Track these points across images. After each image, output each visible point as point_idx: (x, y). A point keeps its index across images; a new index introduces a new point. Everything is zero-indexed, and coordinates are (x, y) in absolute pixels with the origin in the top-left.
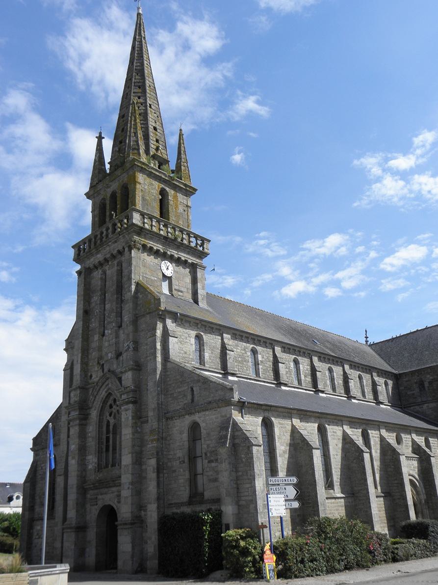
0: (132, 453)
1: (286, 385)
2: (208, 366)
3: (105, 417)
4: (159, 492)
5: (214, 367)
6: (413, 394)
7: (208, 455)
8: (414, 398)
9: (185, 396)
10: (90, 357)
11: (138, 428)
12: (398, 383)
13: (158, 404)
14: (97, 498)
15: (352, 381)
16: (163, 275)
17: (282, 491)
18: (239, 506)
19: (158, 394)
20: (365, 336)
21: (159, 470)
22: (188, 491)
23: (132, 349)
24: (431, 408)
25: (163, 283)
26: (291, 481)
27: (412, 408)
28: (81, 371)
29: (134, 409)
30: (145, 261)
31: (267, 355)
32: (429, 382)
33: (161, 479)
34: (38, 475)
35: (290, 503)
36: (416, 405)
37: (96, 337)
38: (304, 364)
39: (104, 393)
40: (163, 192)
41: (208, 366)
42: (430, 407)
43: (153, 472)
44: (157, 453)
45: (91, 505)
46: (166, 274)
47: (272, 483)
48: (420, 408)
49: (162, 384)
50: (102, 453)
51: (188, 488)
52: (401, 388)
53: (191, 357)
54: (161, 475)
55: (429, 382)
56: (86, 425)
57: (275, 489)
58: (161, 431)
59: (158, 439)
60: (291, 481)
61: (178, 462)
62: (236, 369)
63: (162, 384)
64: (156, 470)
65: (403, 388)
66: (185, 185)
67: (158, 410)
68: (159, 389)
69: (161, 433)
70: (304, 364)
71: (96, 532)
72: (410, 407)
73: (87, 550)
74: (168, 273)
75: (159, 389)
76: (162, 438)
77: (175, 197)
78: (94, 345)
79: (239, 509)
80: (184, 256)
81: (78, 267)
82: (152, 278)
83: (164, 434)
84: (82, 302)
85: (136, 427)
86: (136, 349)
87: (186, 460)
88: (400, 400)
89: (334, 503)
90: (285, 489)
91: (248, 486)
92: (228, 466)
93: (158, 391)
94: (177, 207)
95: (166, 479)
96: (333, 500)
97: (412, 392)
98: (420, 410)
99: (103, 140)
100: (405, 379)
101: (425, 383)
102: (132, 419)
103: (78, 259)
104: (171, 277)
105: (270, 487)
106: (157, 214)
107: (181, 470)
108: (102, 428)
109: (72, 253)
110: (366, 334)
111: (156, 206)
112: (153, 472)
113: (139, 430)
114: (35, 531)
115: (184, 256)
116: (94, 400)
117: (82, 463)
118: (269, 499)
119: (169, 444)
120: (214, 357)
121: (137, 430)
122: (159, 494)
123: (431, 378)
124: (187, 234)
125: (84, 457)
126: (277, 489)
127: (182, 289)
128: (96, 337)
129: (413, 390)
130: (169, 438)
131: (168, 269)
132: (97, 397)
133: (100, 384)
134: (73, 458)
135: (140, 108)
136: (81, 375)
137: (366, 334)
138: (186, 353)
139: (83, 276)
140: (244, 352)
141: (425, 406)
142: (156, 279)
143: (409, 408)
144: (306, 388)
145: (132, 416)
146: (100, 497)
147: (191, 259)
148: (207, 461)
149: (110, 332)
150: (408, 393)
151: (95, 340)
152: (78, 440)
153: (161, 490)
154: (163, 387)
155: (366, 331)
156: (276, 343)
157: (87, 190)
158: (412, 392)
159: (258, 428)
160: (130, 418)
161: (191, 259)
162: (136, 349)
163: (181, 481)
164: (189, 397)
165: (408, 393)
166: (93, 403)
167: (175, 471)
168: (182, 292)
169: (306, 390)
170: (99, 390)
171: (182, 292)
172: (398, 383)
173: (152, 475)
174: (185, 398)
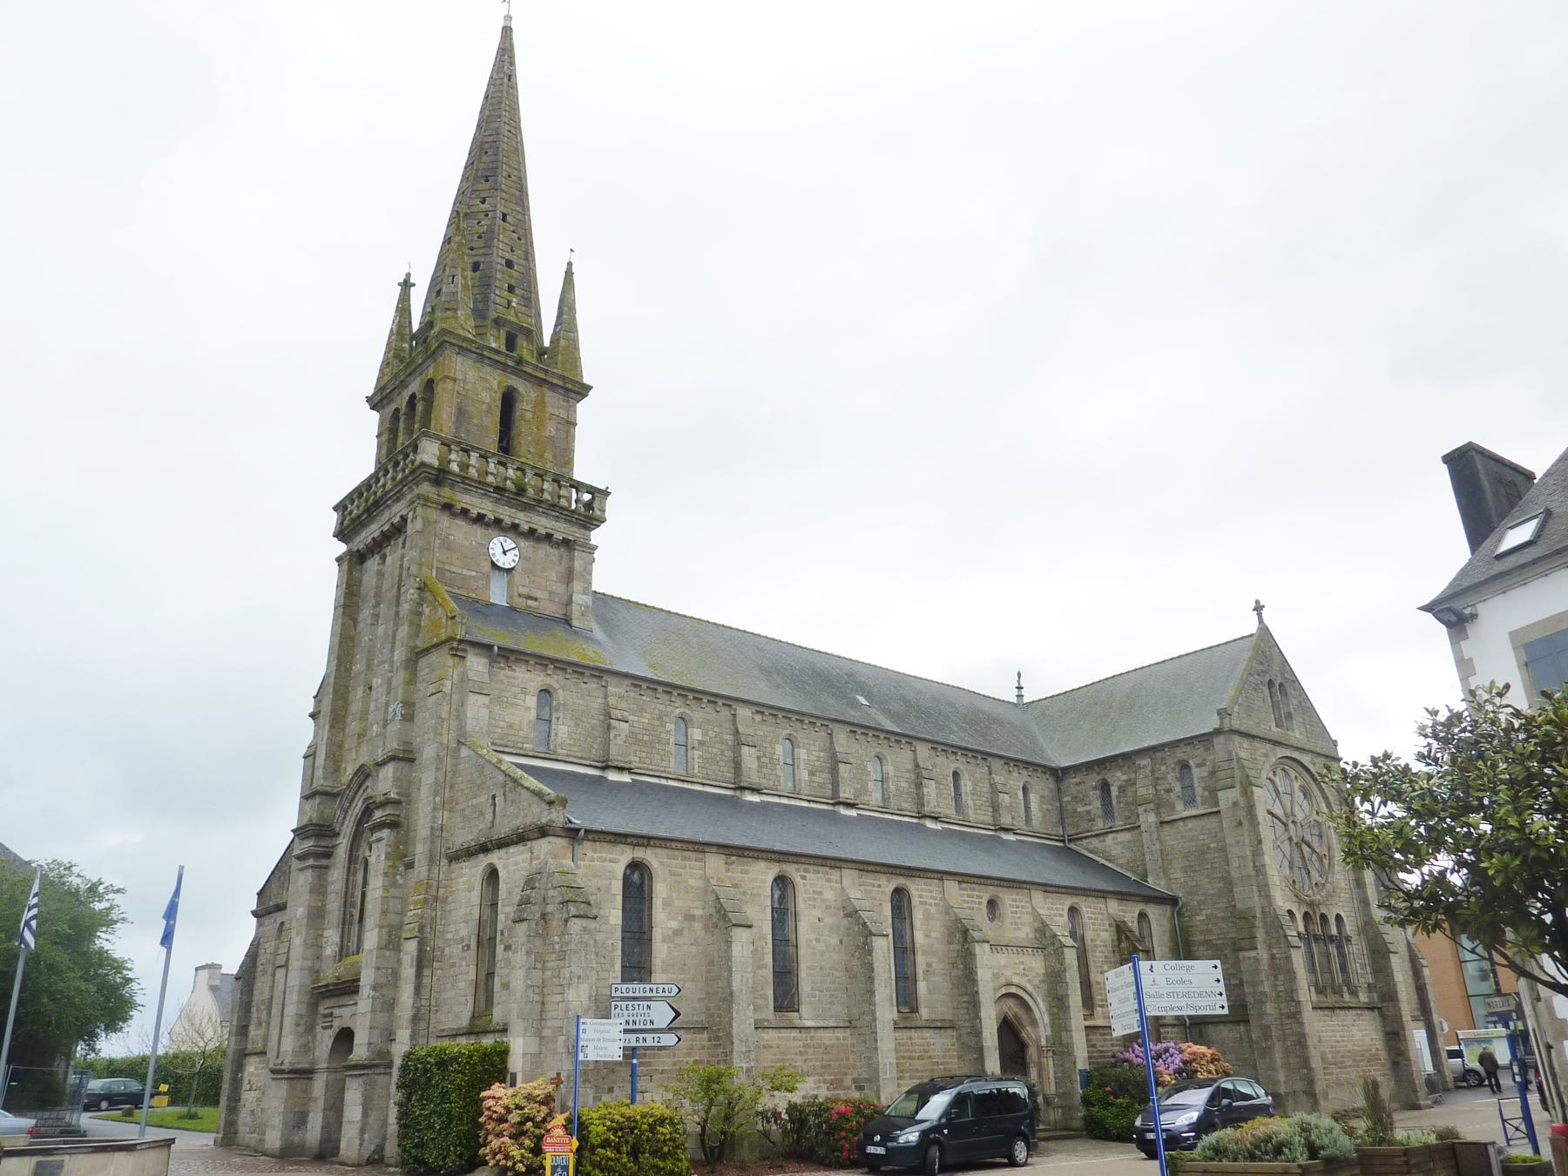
0: (381, 927)
1: (755, 790)
2: (564, 752)
3: (360, 853)
4: (418, 1005)
5: (579, 755)
6: (1088, 812)
7: (506, 934)
8: (1089, 821)
9: (482, 814)
10: (347, 731)
11: (398, 877)
12: (1059, 789)
13: (432, 828)
14: (332, 1013)
15: (933, 782)
16: (494, 565)
17: (641, 1011)
18: (541, 1038)
19: (434, 809)
20: (1017, 685)
21: (421, 963)
22: (470, 1006)
23: (400, 718)
24: (1121, 843)
25: (1539, 475)
26: (664, 991)
27: (1085, 841)
28: (325, 760)
29: (392, 839)
30: (451, 537)
31: (717, 729)
32: (1120, 787)
33: (426, 981)
34: (258, 964)
35: (656, 1036)
36: (1092, 836)
37: (360, 692)
38: (812, 747)
39: (360, 803)
40: (508, 401)
41: (564, 752)
42: (1119, 840)
43: (411, 966)
44: (421, 929)
45: (324, 1028)
46: (500, 564)
47: (618, 994)
48: (1100, 841)
49: (447, 790)
50: (351, 923)
51: (471, 999)
52: (1066, 799)
53: (522, 733)
54: (427, 972)
55: (1120, 787)
56: (327, 867)
57: (624, 1008)
58: (435, 883)
59: (426, 901)
60: (664, 991)
61: (460, 946)
62: (632, 758)
63: (447, 790)
64: (415, 963)
65: (1070, 798)
66: (563, 378)
67: (432, 842)
68: (437, 799)
69: (434, 888)
70: (812, 747)
71: (327, 1081)
72: (1081, 839)
73: (311, 1115)
74: (506, 562)
75: (437, 799)
76: (436, 899)
77: (540, 403)
78: (355, 707)
79: (540, 1045)
80: (543, 524)
81: (342, 548)
82: (465, 572)
83: (441, 891)
84: (340, 620)
85: (395, 875)
86: (409, 718)
87: (473, 945)
88: (1062, 822)
89: (795, 1039)
90: (649, 1007)
91: (559, 998)
92: (525, 958)
93: (435, 803)
94: (541, 423)
95: (438, 980)
96: (794, 1033)
97: (1085, 808)
98: (1099, 845)
99: (412, 288)
100: (1072, 780)
101: (1112, 788)
102: (386, 858)
103: (342, 534)
104: (513, 569)
105: (613, 1003)
106: (491, 443)
107: (464, 963)
108: (355, 875)
109: (332, 520)
110: (1019, 682)
111: (493, 422)
112: (411, 966)
113: (401, 882)
114: (246, 1074)
115: (543, 524)
116: (344, 818)
117: (316, 944)
118: (582, 1027)
119: (450, 911)
120: (580, 734)
121: (396, 881)
122: (419, 1009)
123: (1124, 777)
124: (553, 480)
125: (320, 932)
126: (630, 1007)
127: (538, 594)
128: (360, 692)
129: (1089, 804)
130: (450, 899)
131: (504, 551)
132: (350, 813)
133: (355, 787)
134: (298, 933)
135: (483, 223)
136: (324, 767)
137: (1019, 682)
138: (511, 726)
139: (346, 566)
140: (658, 723)
141: (1109, 839)
142: (474, 574)
143: (1079, 843)
144: (809, 798)
145: (387, 854)
146: (337, 1012)
147: (561, 530)
148: (502, 946)
149: (379, 681)
150: (1079, 810)
151: (358, 697)
152: (308, 898)
153: (424, 1002)
154: (447, 795)
155: (1019, 675)
156: (741, 704)
157: (370, 393)
158: (1085, 808)
159: (614, 882)
160: (383, 857)
161: (561, 530)
162: (409, 718)
163: (462, 985)
164: (489, 817)
165: (1079, 810)
166: (343, 823)
167: (453, 965)
168: (536, 599)
169: (809, 801)
170: (354, 798)
171: (536, 599)
172: (1059, 789)
173: (408, 972)
174: (481, 818)
